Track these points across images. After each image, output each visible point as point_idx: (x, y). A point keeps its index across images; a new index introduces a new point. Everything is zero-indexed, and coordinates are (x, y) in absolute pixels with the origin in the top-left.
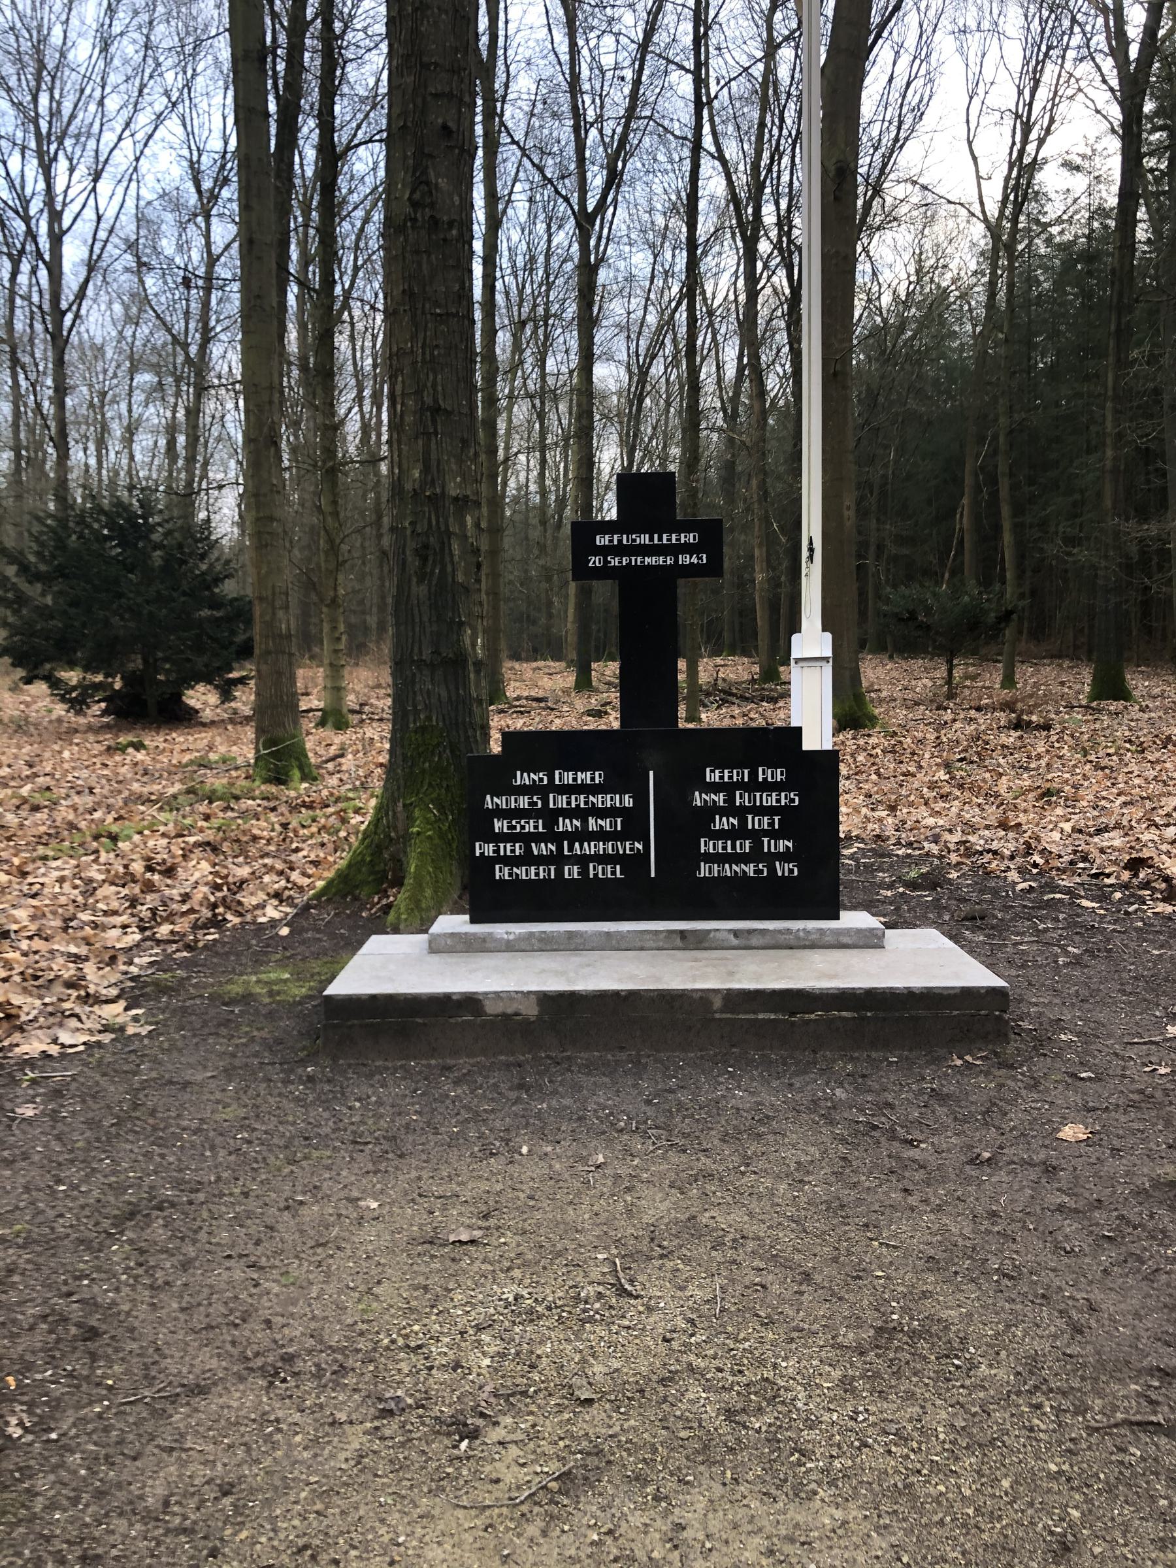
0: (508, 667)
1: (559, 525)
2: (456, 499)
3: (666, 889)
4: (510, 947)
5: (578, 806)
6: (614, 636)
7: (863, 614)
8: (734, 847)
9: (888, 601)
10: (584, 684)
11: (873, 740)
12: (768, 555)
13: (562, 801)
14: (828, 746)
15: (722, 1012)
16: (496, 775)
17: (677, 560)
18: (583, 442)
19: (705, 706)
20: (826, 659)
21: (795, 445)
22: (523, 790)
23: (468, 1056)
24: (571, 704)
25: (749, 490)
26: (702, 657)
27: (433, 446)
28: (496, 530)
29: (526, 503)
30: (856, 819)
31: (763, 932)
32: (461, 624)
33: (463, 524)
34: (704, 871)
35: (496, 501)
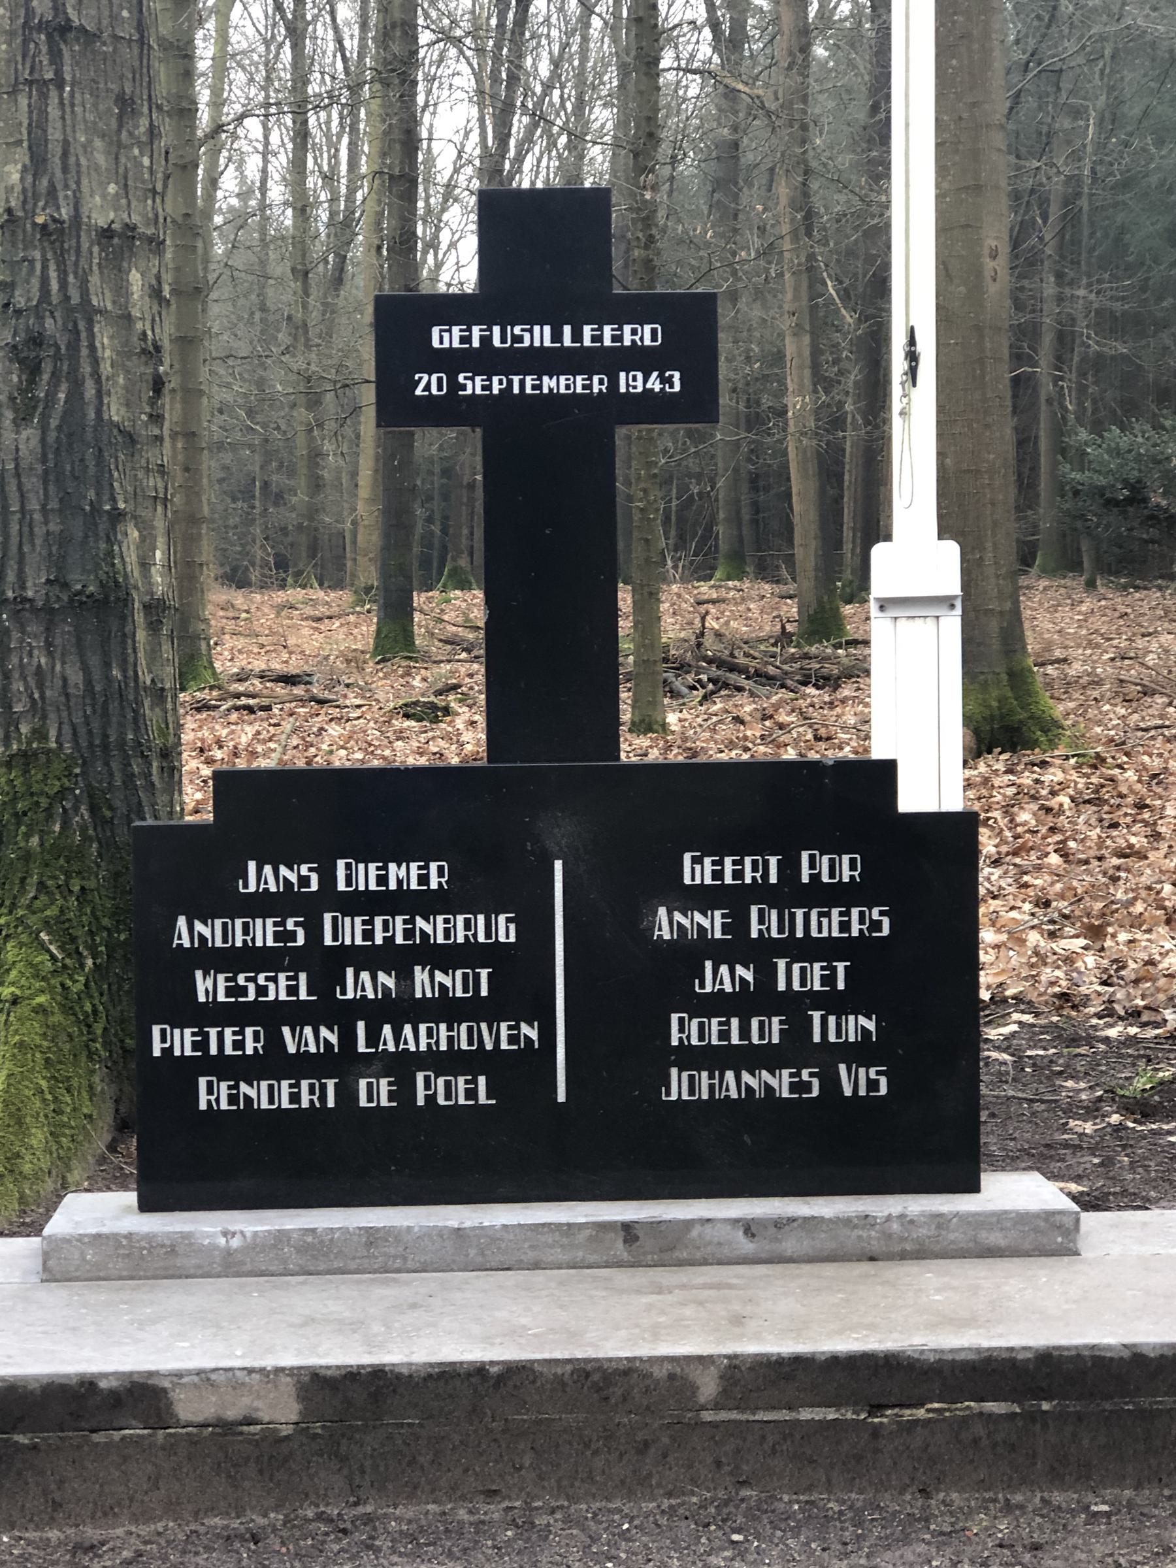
0: (218, 601)
1: (338, 279)
2: (107, 233)
3: (593, 1129)
4: (231, 1265)
5: (389, 941)
6: (471, 533)
7: (1026, 485)
8: (745, 1032)
9: (1081, 460)
10: (396, 639)
11: (1053, 776)
12: (816, 352)
13: (353, 931)
14: (954, 802)
15: (717, 1406)
16: (198, 868)
17: (614, 383)
18: (394, 95)
19: (674, 694)
20: (947, 602)
21: (875, 109)
22: (262, 905)
23: (135, 1519)
24: (366, 691)
25: (769, 206)
26: (665, 579)
27: (53, 111)
28: (193, 293)
29: (263, 231)
30: (1015, 959)
31: (811, 1223)
32: (117, 516)
33: (121, 289)
34: (678, 1086)
35: (192, 226)
